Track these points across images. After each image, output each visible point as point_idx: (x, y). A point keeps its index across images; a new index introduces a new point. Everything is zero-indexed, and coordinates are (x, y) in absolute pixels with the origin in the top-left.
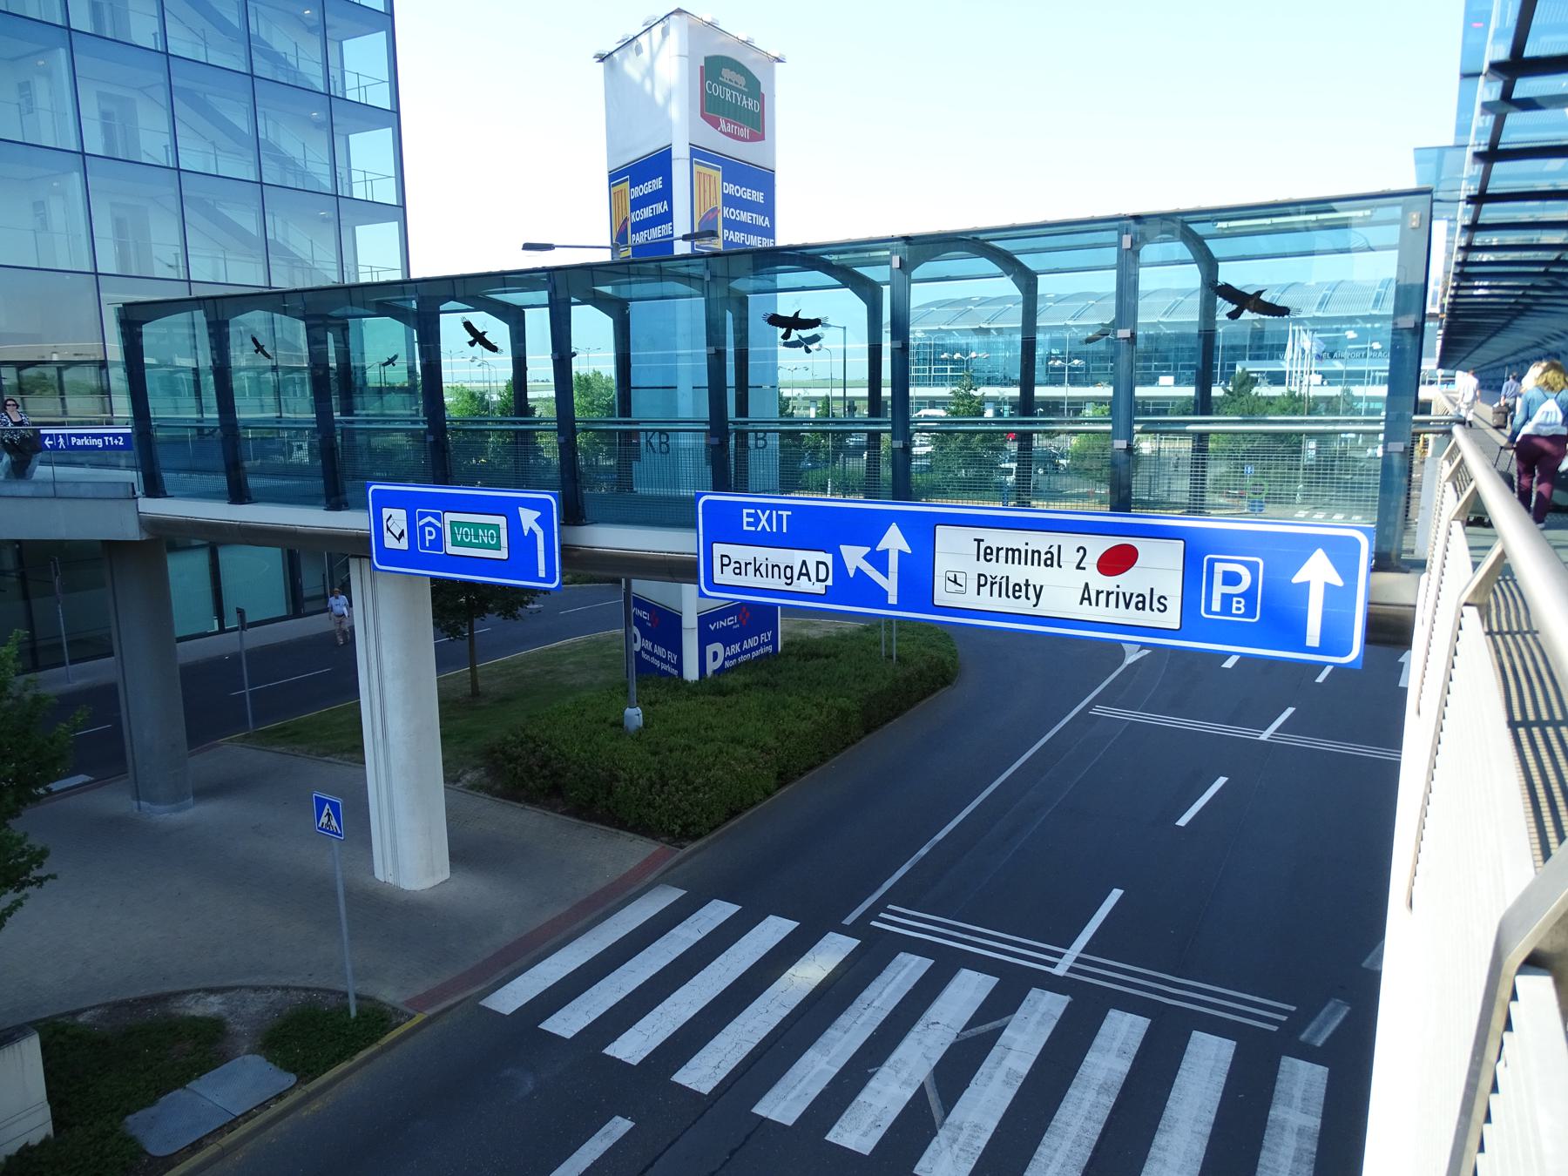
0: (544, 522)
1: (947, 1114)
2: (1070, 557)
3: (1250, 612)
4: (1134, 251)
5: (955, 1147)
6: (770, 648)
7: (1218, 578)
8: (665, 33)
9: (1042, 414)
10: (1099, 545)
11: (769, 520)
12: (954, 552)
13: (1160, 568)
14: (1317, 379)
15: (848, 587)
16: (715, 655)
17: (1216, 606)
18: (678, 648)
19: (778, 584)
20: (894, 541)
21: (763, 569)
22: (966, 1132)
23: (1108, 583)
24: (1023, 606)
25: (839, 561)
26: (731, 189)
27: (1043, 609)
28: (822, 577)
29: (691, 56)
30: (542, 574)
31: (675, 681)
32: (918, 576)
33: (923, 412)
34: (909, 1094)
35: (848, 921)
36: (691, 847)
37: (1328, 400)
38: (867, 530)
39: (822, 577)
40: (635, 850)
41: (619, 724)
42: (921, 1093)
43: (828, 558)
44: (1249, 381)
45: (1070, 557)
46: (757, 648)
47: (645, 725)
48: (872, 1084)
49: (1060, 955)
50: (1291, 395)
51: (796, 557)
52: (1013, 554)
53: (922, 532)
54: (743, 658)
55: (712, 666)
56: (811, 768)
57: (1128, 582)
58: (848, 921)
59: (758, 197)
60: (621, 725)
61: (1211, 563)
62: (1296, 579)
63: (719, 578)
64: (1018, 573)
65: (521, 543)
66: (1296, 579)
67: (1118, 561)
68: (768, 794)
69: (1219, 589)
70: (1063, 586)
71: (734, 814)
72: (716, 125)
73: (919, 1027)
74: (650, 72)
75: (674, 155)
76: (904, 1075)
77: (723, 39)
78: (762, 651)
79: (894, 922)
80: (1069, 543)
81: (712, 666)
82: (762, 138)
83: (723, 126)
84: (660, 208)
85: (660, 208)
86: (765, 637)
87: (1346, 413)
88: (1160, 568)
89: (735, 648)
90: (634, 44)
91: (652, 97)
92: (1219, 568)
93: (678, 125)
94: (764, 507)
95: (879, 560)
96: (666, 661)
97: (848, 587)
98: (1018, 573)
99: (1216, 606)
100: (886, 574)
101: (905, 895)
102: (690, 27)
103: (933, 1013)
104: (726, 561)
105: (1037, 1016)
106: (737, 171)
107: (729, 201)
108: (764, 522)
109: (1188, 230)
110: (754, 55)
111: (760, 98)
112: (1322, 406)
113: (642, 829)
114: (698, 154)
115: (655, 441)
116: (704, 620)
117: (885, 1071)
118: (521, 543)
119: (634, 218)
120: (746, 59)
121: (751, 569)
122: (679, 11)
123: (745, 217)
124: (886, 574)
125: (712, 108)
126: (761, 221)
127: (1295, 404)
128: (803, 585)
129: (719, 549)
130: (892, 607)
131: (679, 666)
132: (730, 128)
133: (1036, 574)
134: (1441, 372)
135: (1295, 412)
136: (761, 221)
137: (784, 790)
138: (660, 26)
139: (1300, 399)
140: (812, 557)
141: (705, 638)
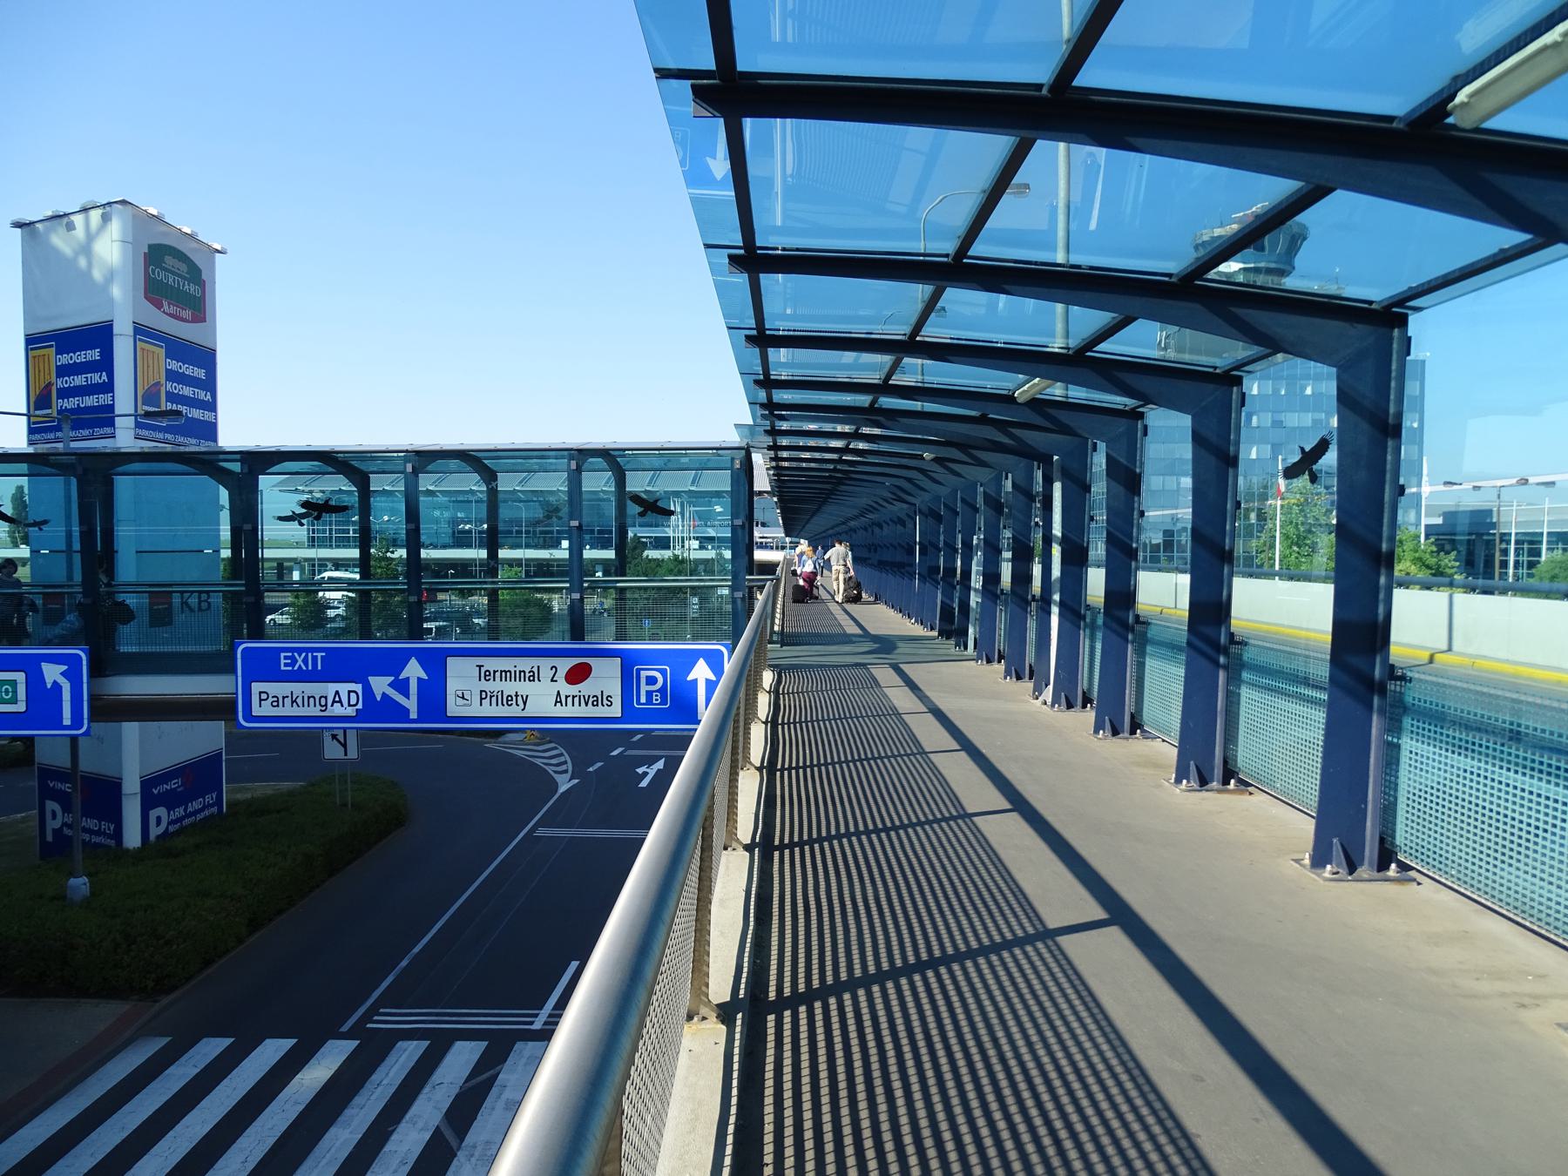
0: (72, 675)
1: (462, 1140)
2: (546, 673)
3: (664, 702)
4: (579, 470)
5: (473, 1160)
6: (215, 810)
7: (643, 681)
8: (106, 218)
9: (453, 576)
10: (565, 665)
11: (305, 661)
12: (462, 678)
13: (606, 677)
14: (695, 544)
15: (374, 708)
16: (159, 820)
17: (643, 700)
18: (116, 817)
19: (315, 711)
20: (414, 671)
21: (299, 701)
22: (479, 1149)
23: (572, 690)
24: (514, 711)
25: (368, 690)
26: (174, 365)
27: (529, 712)
28: (353, 701)
29: (135, 243)
30: (67, 721)
31: (118, 852)
32: (433, 694)
33: (326, 575)
34: (427, 1136)
35: (345, 1028)
36: (165, 1000)
37: (706, 561)
38: (392, 664)
39: (353, 701)
40: (102, 1014)
41: (61, 897)
42: (437, 1133)
43: (358, 688)
44: (640, 545)
45: (546, 673)
46: (202, 810)
47: (92, 894)
48: (394, 1137)
49: (536, 1016)
50: (676, 557)
51: (331, 689)
52: (506, 675)
53: (435, 664)
54: (186, 822)
55: (155, 832)
56: (280, 912)
57: (586, 688)
58: (345, 1028)
59: (200, 373)
60: (64, 897)
61: (638, 671)
62: (690, 678)
63: (257, 711)
64: (510, 688)
65: (43, 701)
66: (690, 678)
67: (578, 675)
68: (240, 941)
69: (644, 688)
70: (544, 694)
71: (208, 963)
72: (159, 306)
73: (426, 1090)
74: (86, 249)
75: (116, 331)
76: (420, 1124)
77: (164, 228)
78: (206, 813)
79: (386, 1021)
80: (545, 664)
81: (155, 832)
82: (204, 320)
83: (166, 307)
84: (96, 378)
85: (96, 378)
86: (210, 798)
87: (720, 573)
88: (606, 677)
89: (180, 812)
90: (65, 220)
91: (87, 275)
92: (644, 674)
93: (122, 305)
94: (299, 651)
95: (402, 686)
96: (98, 833)
97: (374, 708)
98: (510, 688)
99: (643, 700)
100: (407, 696)
101: (394, 998)
102: (134, 216)
103: (437, 1077)
104: (264, 696)
105: (524, 1060)
106: (179, 349)
107: (172, 376)
108: (300, 662)
109: (612, 458)
110: (194, 245)
111: (202, 284)
112: (701, 567)
113: (110, 991)
114: (140, 331)
115: (193, 601)
116: (147, 784)
117: (403, 1127)
118: (43, 701)
119: (62, 383)
120: (186, 247)
121: (288, 701)
122: (123, 202)
123: (187, 391)
124: (407, 696)
125: (155, 291)
126: (203, 395)
127: (679, 565)
128: (337, 710)
129: (256, 687)
130: (414, 721)
131: (118, 835)
132: (172, 310)
133: (523, 688)
134: (788, 540)
135: (680, 573)
136: (203, 395)
137: (257, 935)
138: (99, 211)
139: (683, 561)
140: (344, 688)
141: (148, 803)
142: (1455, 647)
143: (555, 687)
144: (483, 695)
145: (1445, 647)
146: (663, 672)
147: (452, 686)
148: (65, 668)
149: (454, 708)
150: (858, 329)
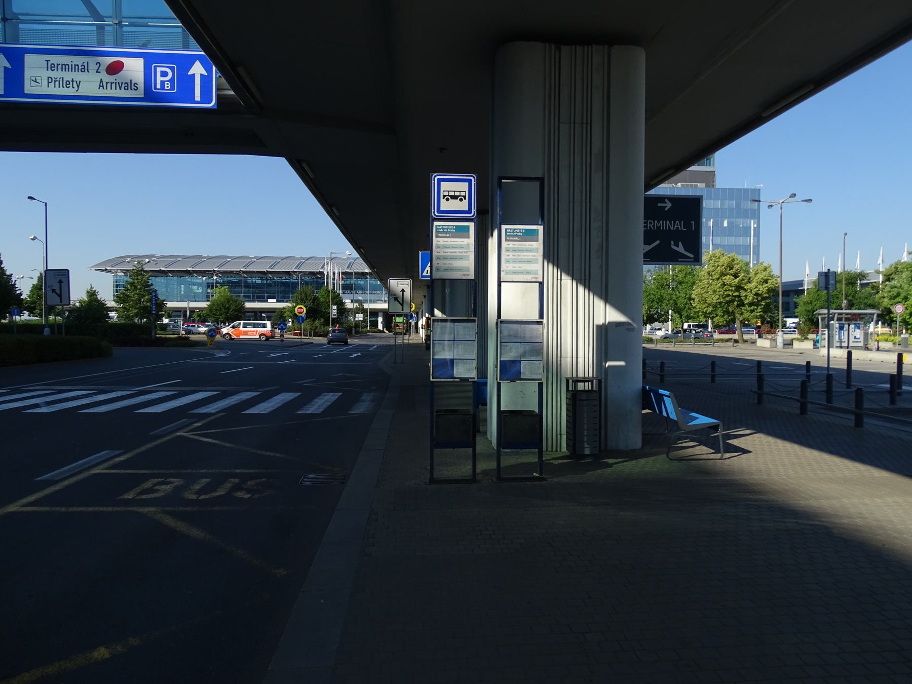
2: (93, 67)
3: (172, 88)
7: (159, 74)
17: (159, 86)
23: (111, 78)
45: (93, 67)
61: (155, 67)
64: (68, 76)
69: (159, 79)
92: (159, 70)
99: (159, 86)
130: (197, 102)
133: (77, 76)
142: (540, 176)
143: (97, 77)
144: (50, 80)
145: (436, 475)
146: (172, 69)
147: (28, 73)
148: (9, 66)
149: (29, 88)
150: (157, 16)
